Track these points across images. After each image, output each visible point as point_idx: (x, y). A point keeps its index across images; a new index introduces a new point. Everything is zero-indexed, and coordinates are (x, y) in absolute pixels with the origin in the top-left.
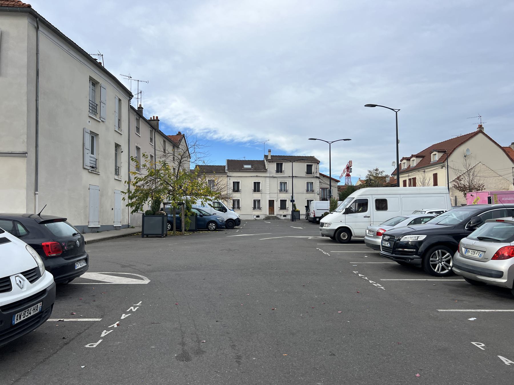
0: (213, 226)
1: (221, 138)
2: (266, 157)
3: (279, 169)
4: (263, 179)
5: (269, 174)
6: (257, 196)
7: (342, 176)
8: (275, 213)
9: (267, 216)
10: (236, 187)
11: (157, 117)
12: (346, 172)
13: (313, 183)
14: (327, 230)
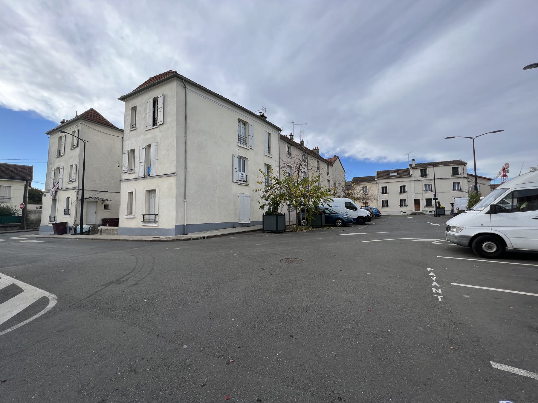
0: (340, 223)
1: (389, 161)
2: (411, 165)
3: (424, 173)
4: (408, 183)
5: (413, 179)
6: (403, 196)
7: (497, 177)
8: (421, 210)
9: (413, 212)
10: (385, 191)
11: (317, 147)
12: (502, 173)
13: (460, 182)
14: (456, 237)
